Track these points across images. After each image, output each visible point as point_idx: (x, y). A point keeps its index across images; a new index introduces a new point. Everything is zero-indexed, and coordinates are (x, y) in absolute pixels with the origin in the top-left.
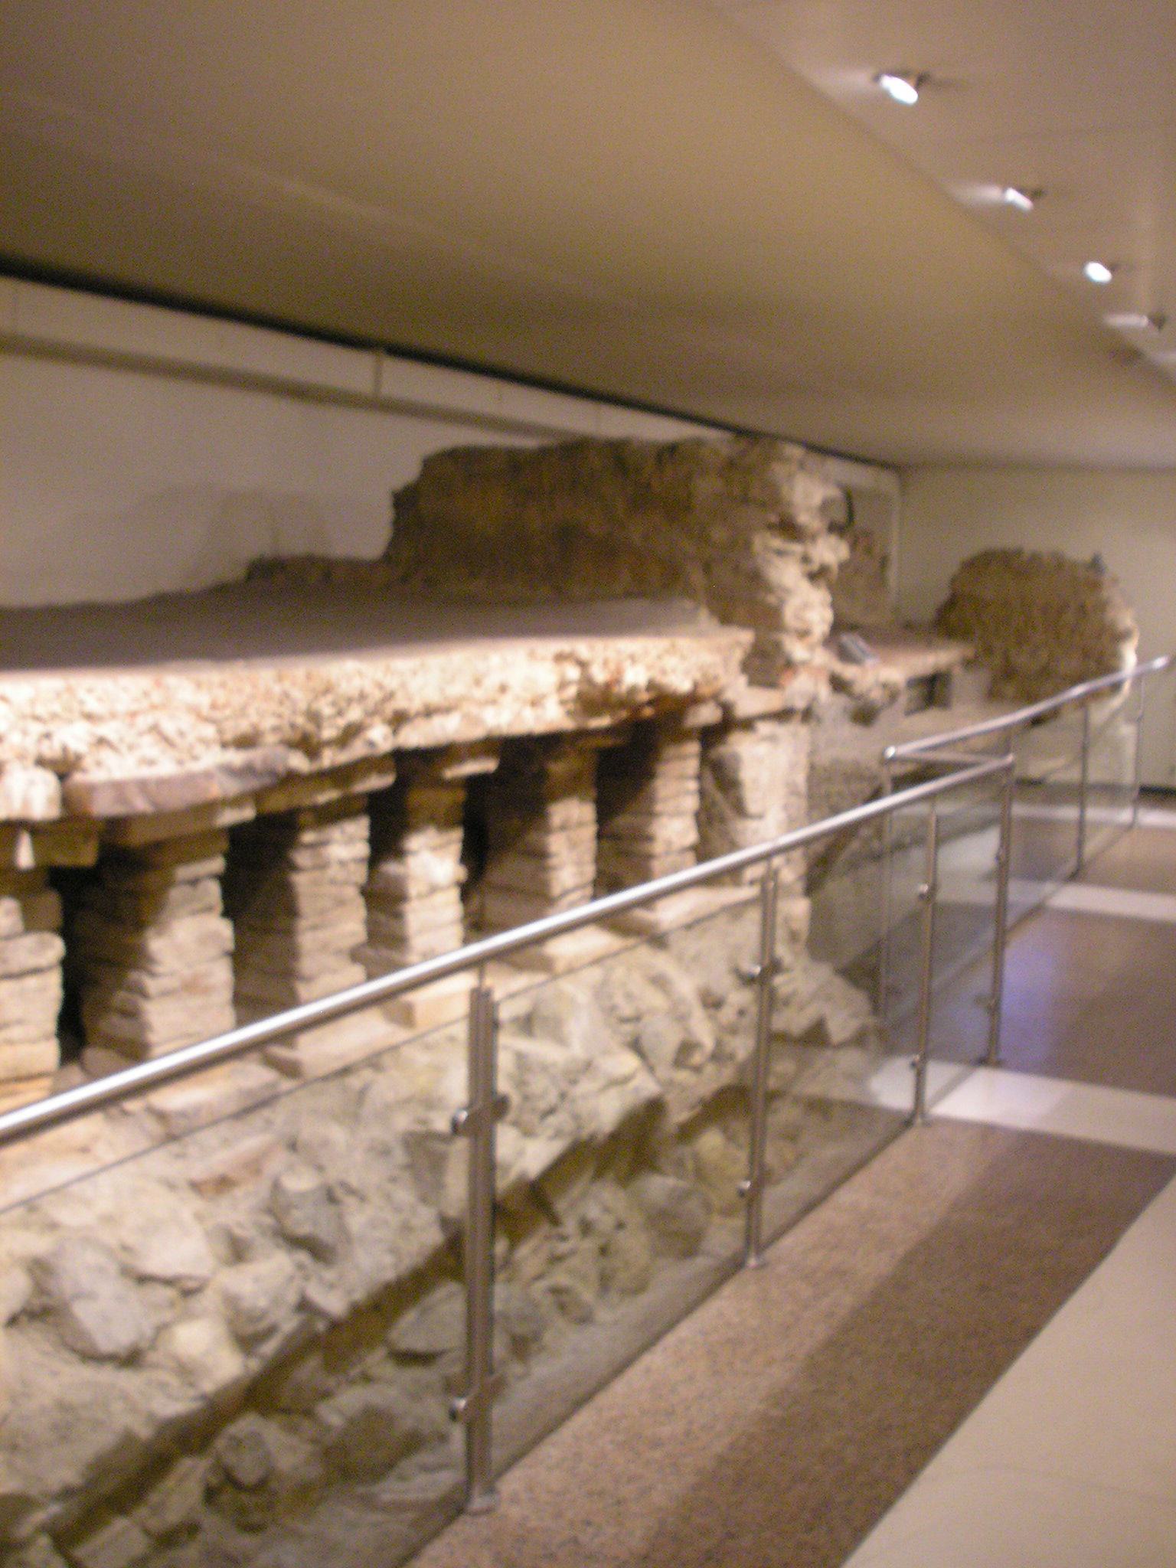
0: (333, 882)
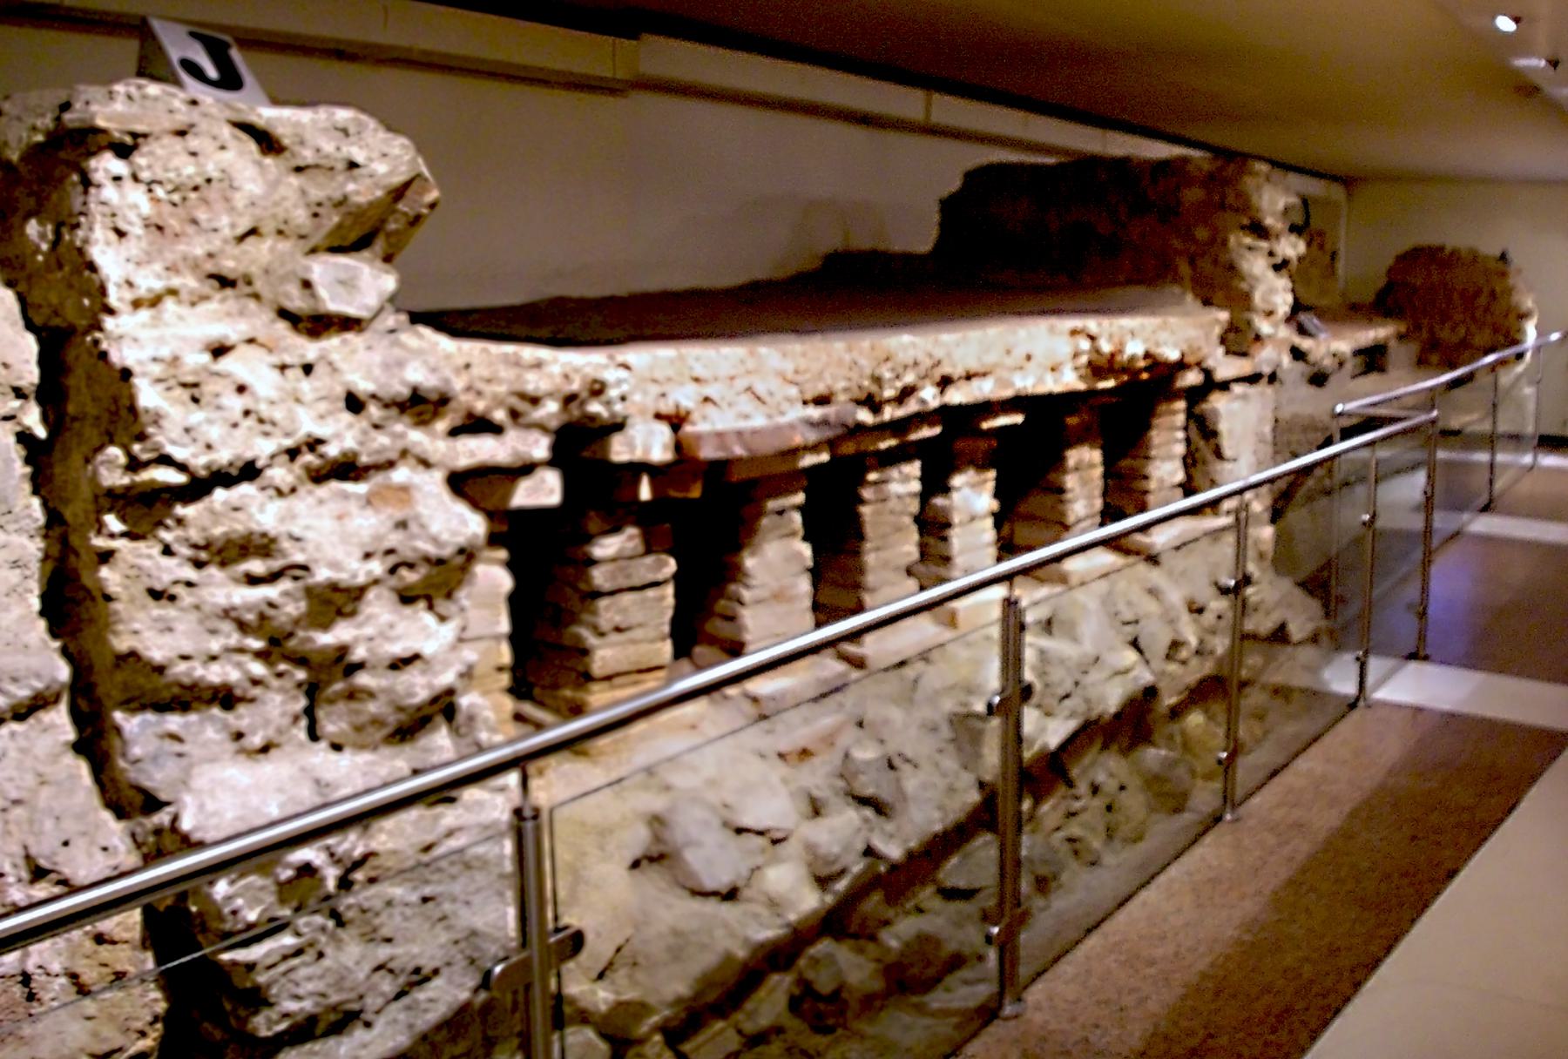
0: (892, 512)
